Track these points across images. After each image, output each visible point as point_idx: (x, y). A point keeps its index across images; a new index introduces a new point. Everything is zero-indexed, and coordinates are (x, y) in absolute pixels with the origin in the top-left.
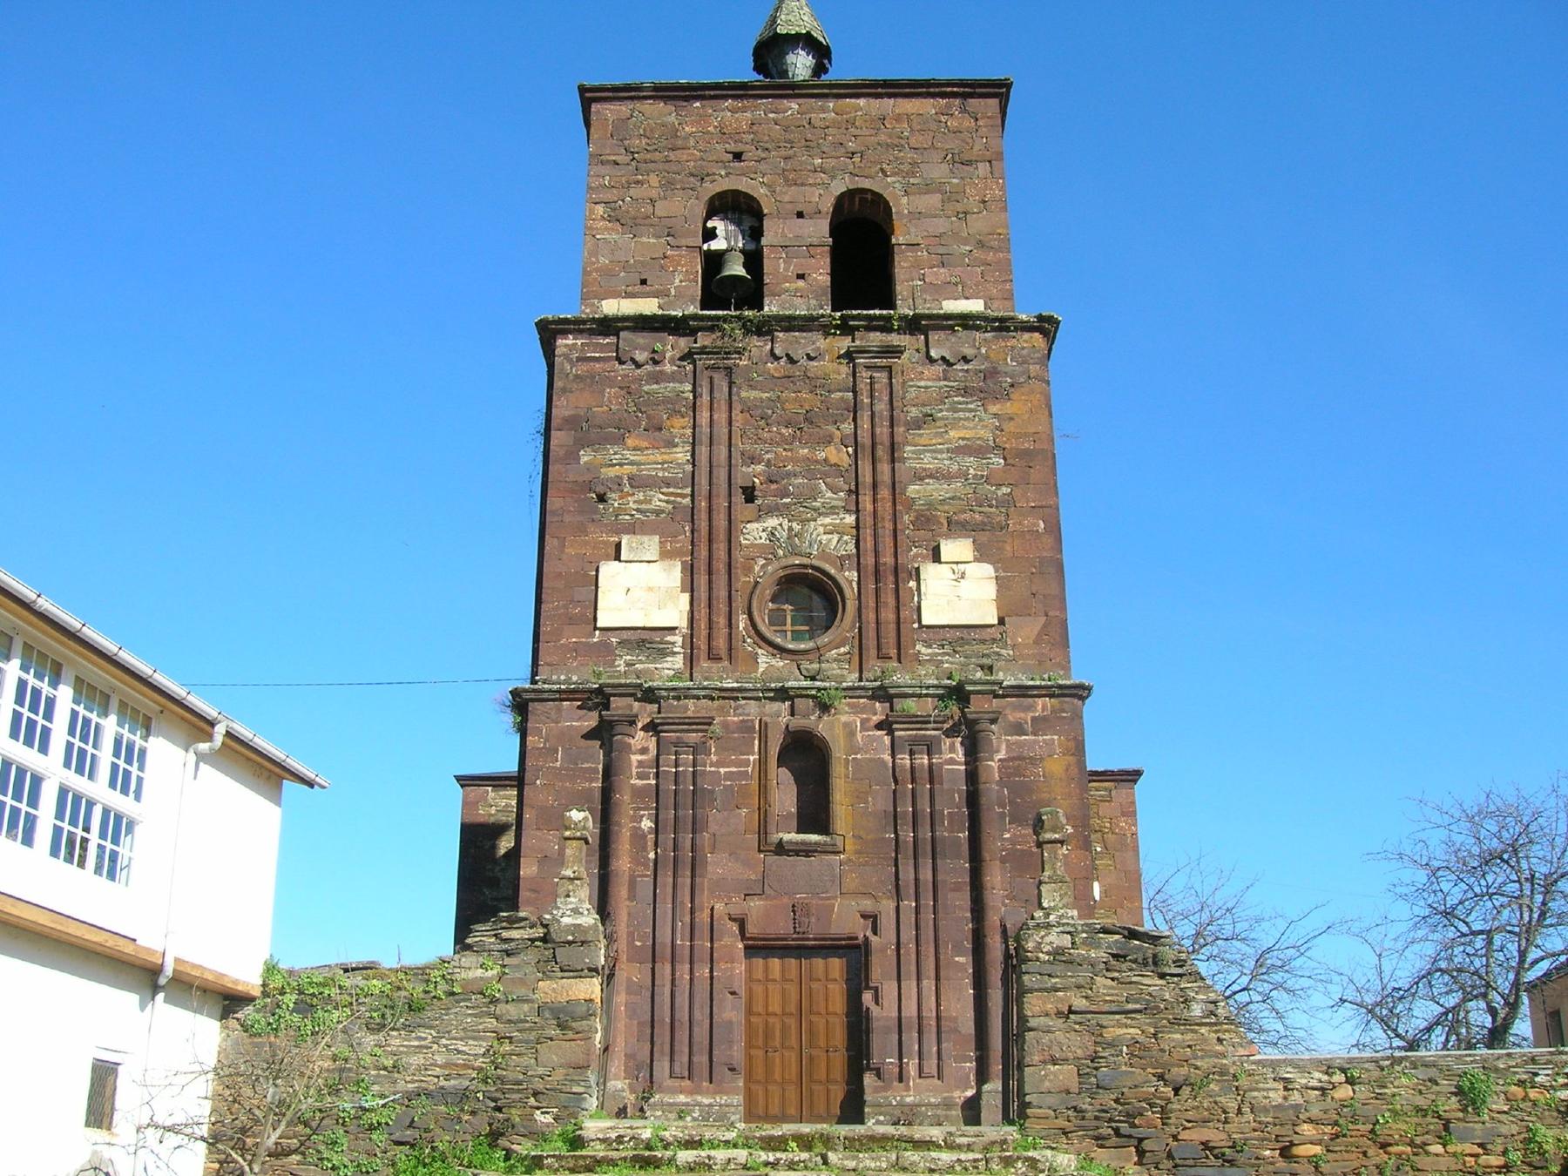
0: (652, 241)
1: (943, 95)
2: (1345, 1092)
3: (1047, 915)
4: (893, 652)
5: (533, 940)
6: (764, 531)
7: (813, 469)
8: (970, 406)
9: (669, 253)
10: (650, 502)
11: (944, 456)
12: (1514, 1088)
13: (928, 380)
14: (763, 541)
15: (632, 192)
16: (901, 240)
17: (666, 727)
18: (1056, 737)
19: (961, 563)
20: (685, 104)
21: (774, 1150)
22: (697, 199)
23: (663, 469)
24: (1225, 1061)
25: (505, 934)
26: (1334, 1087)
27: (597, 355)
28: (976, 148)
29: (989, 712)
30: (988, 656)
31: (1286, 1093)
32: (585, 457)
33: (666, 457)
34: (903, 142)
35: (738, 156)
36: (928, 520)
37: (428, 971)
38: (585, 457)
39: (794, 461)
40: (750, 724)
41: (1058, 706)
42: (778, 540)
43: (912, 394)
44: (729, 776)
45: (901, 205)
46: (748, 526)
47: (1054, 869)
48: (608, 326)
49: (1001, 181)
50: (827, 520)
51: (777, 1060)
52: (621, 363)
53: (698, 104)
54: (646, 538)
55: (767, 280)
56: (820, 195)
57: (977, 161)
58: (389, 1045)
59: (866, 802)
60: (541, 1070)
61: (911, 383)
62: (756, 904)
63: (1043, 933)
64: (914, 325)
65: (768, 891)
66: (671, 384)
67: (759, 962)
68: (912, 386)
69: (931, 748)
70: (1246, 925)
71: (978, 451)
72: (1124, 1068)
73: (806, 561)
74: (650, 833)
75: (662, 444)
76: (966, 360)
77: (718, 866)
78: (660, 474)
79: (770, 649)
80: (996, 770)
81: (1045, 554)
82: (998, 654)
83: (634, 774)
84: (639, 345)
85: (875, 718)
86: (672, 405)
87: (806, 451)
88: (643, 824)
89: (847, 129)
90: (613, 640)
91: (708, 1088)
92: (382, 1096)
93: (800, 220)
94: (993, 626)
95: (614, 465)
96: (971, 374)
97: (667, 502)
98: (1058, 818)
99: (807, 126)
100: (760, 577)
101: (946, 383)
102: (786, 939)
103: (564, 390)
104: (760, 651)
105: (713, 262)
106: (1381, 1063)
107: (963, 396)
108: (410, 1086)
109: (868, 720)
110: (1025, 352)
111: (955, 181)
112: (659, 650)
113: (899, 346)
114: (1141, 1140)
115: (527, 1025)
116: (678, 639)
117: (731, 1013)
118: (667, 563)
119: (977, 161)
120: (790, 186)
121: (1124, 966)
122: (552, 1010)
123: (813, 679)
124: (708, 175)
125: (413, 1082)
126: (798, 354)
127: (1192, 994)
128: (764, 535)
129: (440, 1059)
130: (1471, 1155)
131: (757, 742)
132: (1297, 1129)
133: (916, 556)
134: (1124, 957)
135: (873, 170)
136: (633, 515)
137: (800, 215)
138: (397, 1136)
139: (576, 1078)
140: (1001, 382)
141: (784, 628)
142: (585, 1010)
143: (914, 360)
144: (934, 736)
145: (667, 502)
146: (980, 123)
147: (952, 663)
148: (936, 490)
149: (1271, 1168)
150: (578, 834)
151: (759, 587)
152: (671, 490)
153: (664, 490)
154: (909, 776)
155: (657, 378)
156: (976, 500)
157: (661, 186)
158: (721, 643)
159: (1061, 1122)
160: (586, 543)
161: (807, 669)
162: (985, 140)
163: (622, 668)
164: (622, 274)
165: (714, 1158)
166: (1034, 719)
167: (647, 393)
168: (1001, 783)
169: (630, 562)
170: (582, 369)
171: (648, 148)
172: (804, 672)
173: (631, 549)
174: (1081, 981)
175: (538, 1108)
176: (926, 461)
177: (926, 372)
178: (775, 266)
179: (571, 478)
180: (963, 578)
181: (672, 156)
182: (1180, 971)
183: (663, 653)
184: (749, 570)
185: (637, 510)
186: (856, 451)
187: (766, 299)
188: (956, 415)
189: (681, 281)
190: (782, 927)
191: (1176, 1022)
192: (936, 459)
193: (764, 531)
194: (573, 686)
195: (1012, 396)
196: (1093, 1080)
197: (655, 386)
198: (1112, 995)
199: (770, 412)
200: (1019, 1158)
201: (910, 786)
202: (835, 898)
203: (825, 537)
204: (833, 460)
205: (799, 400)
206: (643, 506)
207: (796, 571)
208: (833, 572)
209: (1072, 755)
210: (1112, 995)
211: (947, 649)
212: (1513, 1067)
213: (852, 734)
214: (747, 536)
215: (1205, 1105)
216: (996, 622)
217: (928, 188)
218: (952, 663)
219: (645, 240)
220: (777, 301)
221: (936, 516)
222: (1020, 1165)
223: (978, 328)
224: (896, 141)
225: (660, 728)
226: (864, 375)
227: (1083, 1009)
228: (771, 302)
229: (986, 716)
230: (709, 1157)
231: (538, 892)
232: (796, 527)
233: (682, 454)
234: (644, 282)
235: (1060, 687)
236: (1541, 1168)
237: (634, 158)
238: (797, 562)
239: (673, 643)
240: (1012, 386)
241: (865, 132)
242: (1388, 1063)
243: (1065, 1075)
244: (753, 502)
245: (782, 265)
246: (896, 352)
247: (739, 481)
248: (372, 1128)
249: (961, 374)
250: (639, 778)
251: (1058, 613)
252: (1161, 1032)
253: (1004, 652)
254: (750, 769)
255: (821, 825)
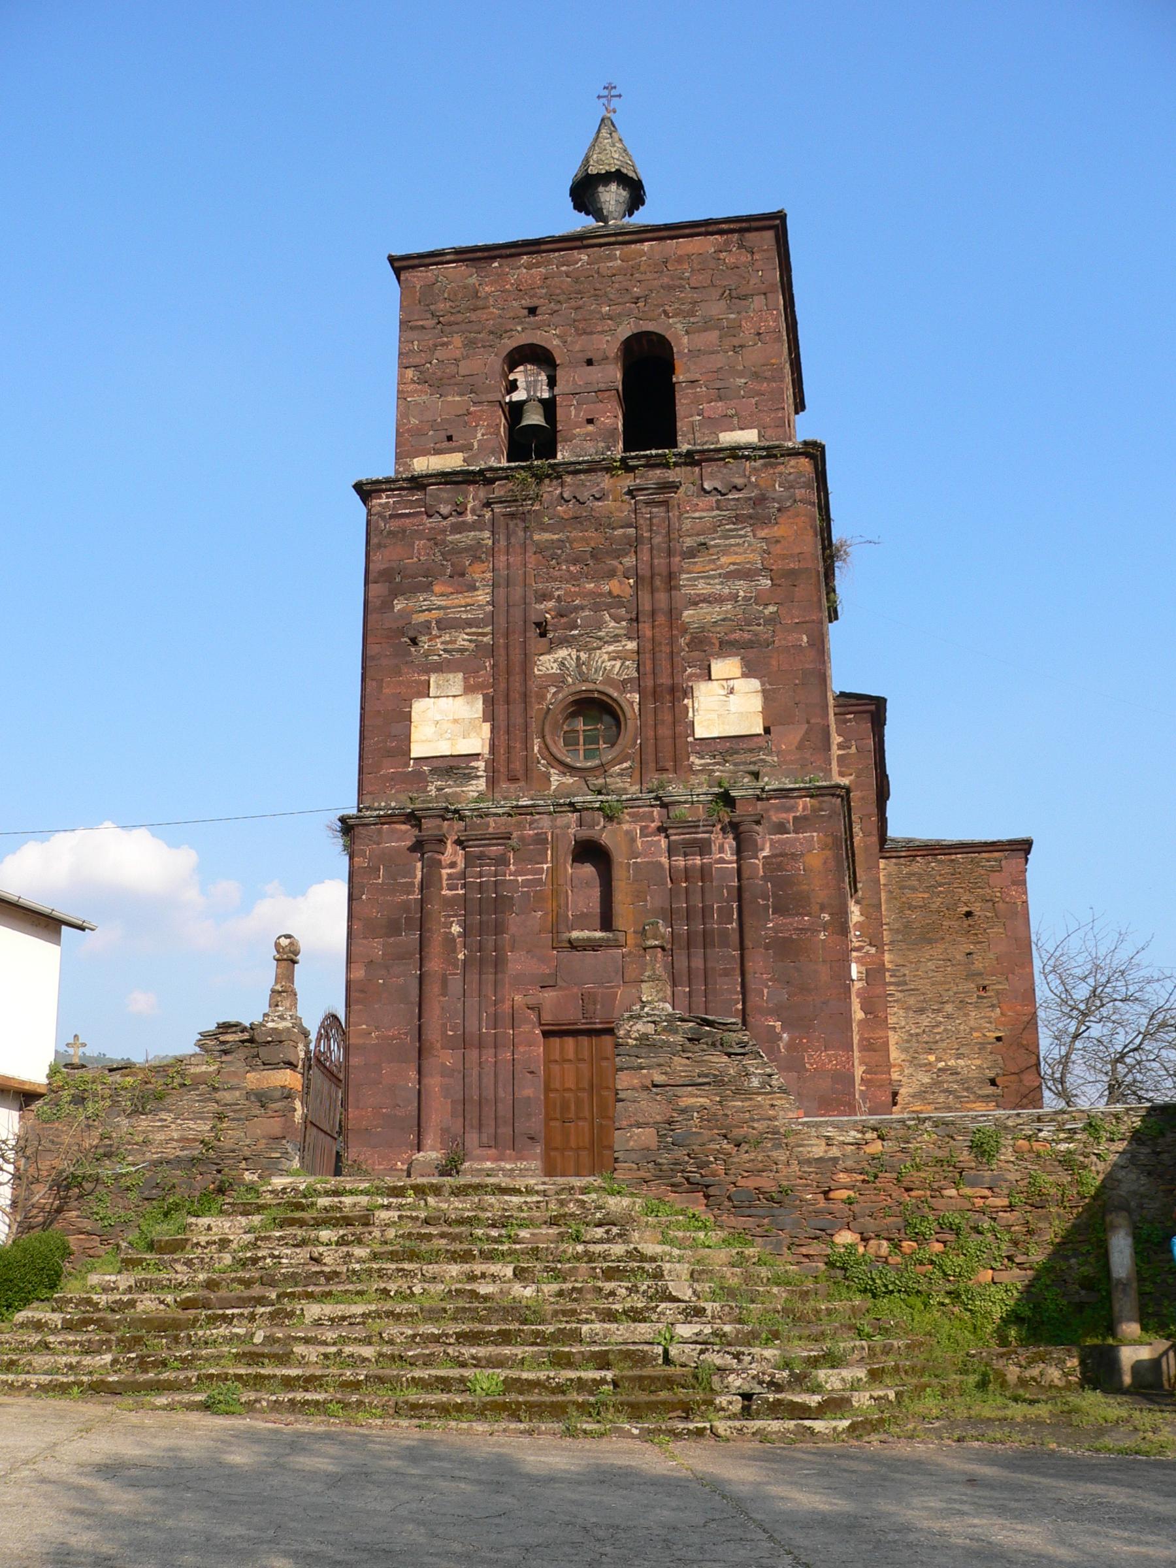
0: (457, 399)
1: (721, 232)
2: (877, 1147)
3: (642, 1008)
4: (669, 765)
5: (243, 1042)
6: (555, 661)
7: (600, 603)
8: (740, 533)
9: (472, 409)
10: (454, 642)
11: (717, 581)
12: (1021, 1142)
13: (703, 510)
14: (554, 671)
15: (438, 354)
16: (681, 378)
17: (471, 843)
18: (815, 834)
19: (730, 679)
20: (485, 265)
21: (397, 1196)
22: (496, 355)
23: (466, 611)
24: (776, 1123)
25: (222, 1038)
26: (867, 1143)
27: (407, 511)
28: (752, 282)
29: (751, 815)
30: (755, 763)
31: (827, 1148)
32: (399, 605)
33: (468, 600)
34: (684, 283)
35: (532, 311)
36: (701, 642)
37: (167, 1069)
38: (399, 605)
39: (584, 595)
40: (544, 836)
41: (817, 805)
42: (568, 669)
43: (687, 525)
44: (526, 883)
45: (682, 343)
46: (541, 658)
47: (653, 969)
48: (417, 483)
49: (775, 312)
50: (611, 648)
51: (573, 1130)
52: (430, 516)
53: (496, 264)
54: (451, 676)
55: (559, 428)
56: (608, 341)
57: (753, 295)
58: (139, 1126)
59: (646, 901)
60: (248, 1142)
61: (687, 515)
62: (549, 995)
63: (631, 1023)
64: (691, 459)
65: (560, 982)
66: (473, 533)
67: (556, 1042)
68: (687, 518)
69: (703, 848)
70: (1136, 987)
71: (747, 574)
72: (694, 1130)
73: (591, 686)
74: (459, 937)
75: (465, 589)
76: (736, 488)
77: (518, 963)
78: (464, 616)
79: (562, 768)
80: (761, 866)
81: (807, 666)
82: (763, 760)
83: (445, 885)
84: (443, 499)
85: (653, 825)
86: (475, 552)
87: (592, 585)
88: (453, 929)
89: (632, 275)
90: (425, 768)
91: (510, 1155)
92: (134, 1165)
93: (590, 367)
94: (759, 735)
95: (424, 611)
96: (742, 502)
97: (470, 641)
98: (658, 928)
99: (596, 276)
100: (551, 704)
101: (718, 512)
102: (576, 1024)
103: (379, 546)
104: (552, 771)
105: (515, 411)
106: (908, 1122)
107: (734, 524)
108: (155, 1156)
109: (647, 827)
110: (792, 477)
111: (732, 316)
112: (465, 774)
113: (673, 482)
114: (707, 1186)
115: (239, 1107)
116: (481, 765)
117: (530, 1090)
118: (470, 697)
119: (753, 295)
120: (581, 335)
121: (696, 1048)
122: (256, 1095)
123: (600, 793)
124: (506, 332)
125: (157, 1153)
126: (584, 495)
127: (752, 1069)
128: (555, 665)
129: (176, 1135)
130: (982, 1197)
131: (549, 852)
132: (835, 1177)
133: (691, 675)
134: (698, 1040)
135: (656, 313)
136: (440, 655)
137: (590, 362)
138: (146, 1194)
139: (274, 1146)
140: (768, 508)
141: (577, 747)
142: (288, 1095)
143: (689, 494)
144: (705, 839)
145: (470, 641)
146: (756, 257)
147: (722, 771)
148: (710, 614)
149: (811, 1208)
150: (285, 957)
151: (551, 712)
152: (474, 630)
153: (468, 630)
154: (684, 876)
155: (458, 528)
156: (745, 621)
157: (465, 346)
158: (517, 766)
159: (642, 1174)
160: (400, 683)
161: (594, 784)
162: (760, 273)
163: (433, 793)
164: (431, 433)
165: (344, 1203)
166: (795, 818)
167: (452, 543)
168: (765, 878)
169: (438, 697)
170: (394, 525)
171: (453, 311)
172: (592, 787)
173: (438, 687)
174: (661, 1060)
175: (247, 1170)
176: (700, 587)
177: (700, 504)
178: (568, 414)
179: (387, 626)
180: (731, 693)
181: (473, 316)
182: (742, 1051)
183: (470, 777)
184: (543, 697)
185: (445, 650)
186: (636, 582)
187: (559, 445)
188: (727, 542)
189: (483, 435)
190: (572, 1015)
191: (738, 1092)
192: (709, 584)
193: (555, 661)
194: (390, 812)
195: (779, 520)
196: (670, 1139)
197: (458, 536)
198: (686, 1071)
199: (559, 552)
200: (571, 1200)
201: (700, 884)
202: (618, 987)
203: (609, 664)
204: (616, 592)
205: (586, 539)
206: (449, 647)
207: (583, 696)
208: (615, 695)
209: (830, 849)
210: (686, 1071)
211: (719, 759)
212: (1021, 1125)
213: (633, 840)
214: (540, 668)
215: (759, 1158)
216: (762, 732)
217: (708, 324)
218: (722, 771)
219: (450, 398)
220: (569, 446)
221: (707, 637)
222: (571, 1205)
223: (748, 458)
224: (677, 282)
225: (466, 844)
226: (644, 510)
227: (663, 1083)
228: (563, 448)
229: (749, 819)
230: (340, 1202)
231: (365, 992)
232: (584, 656)
233: (482, 596)
234: (450, 438)
235: (819, 788)
236: (1042, 1207)
237: (439, 322)
238: (584, 688)
239: (477, 768)
240: (779, 510)
241: (649, 276)
242: (912, 1123)
243: (646, 1137)
244: (545, 636)
245: (573, 413)
246: (674, 487)
247: (534, 618)
248: (128, 1189)
249: (732, 503)
250: (449, 889)
251: (819, 720)
252: (726, 1100)
253: (768, 758)
254: (544, 876)
255: (607, 922)
